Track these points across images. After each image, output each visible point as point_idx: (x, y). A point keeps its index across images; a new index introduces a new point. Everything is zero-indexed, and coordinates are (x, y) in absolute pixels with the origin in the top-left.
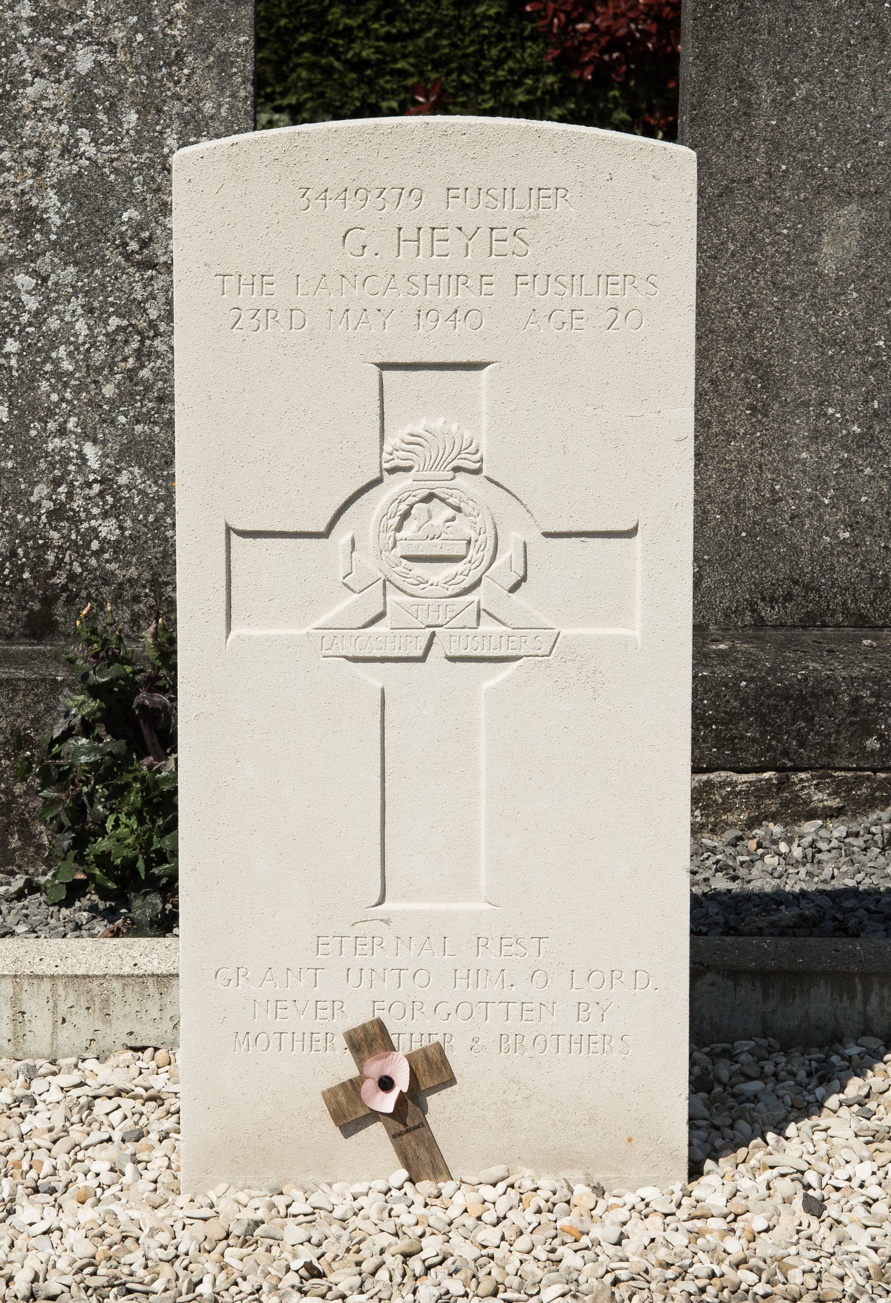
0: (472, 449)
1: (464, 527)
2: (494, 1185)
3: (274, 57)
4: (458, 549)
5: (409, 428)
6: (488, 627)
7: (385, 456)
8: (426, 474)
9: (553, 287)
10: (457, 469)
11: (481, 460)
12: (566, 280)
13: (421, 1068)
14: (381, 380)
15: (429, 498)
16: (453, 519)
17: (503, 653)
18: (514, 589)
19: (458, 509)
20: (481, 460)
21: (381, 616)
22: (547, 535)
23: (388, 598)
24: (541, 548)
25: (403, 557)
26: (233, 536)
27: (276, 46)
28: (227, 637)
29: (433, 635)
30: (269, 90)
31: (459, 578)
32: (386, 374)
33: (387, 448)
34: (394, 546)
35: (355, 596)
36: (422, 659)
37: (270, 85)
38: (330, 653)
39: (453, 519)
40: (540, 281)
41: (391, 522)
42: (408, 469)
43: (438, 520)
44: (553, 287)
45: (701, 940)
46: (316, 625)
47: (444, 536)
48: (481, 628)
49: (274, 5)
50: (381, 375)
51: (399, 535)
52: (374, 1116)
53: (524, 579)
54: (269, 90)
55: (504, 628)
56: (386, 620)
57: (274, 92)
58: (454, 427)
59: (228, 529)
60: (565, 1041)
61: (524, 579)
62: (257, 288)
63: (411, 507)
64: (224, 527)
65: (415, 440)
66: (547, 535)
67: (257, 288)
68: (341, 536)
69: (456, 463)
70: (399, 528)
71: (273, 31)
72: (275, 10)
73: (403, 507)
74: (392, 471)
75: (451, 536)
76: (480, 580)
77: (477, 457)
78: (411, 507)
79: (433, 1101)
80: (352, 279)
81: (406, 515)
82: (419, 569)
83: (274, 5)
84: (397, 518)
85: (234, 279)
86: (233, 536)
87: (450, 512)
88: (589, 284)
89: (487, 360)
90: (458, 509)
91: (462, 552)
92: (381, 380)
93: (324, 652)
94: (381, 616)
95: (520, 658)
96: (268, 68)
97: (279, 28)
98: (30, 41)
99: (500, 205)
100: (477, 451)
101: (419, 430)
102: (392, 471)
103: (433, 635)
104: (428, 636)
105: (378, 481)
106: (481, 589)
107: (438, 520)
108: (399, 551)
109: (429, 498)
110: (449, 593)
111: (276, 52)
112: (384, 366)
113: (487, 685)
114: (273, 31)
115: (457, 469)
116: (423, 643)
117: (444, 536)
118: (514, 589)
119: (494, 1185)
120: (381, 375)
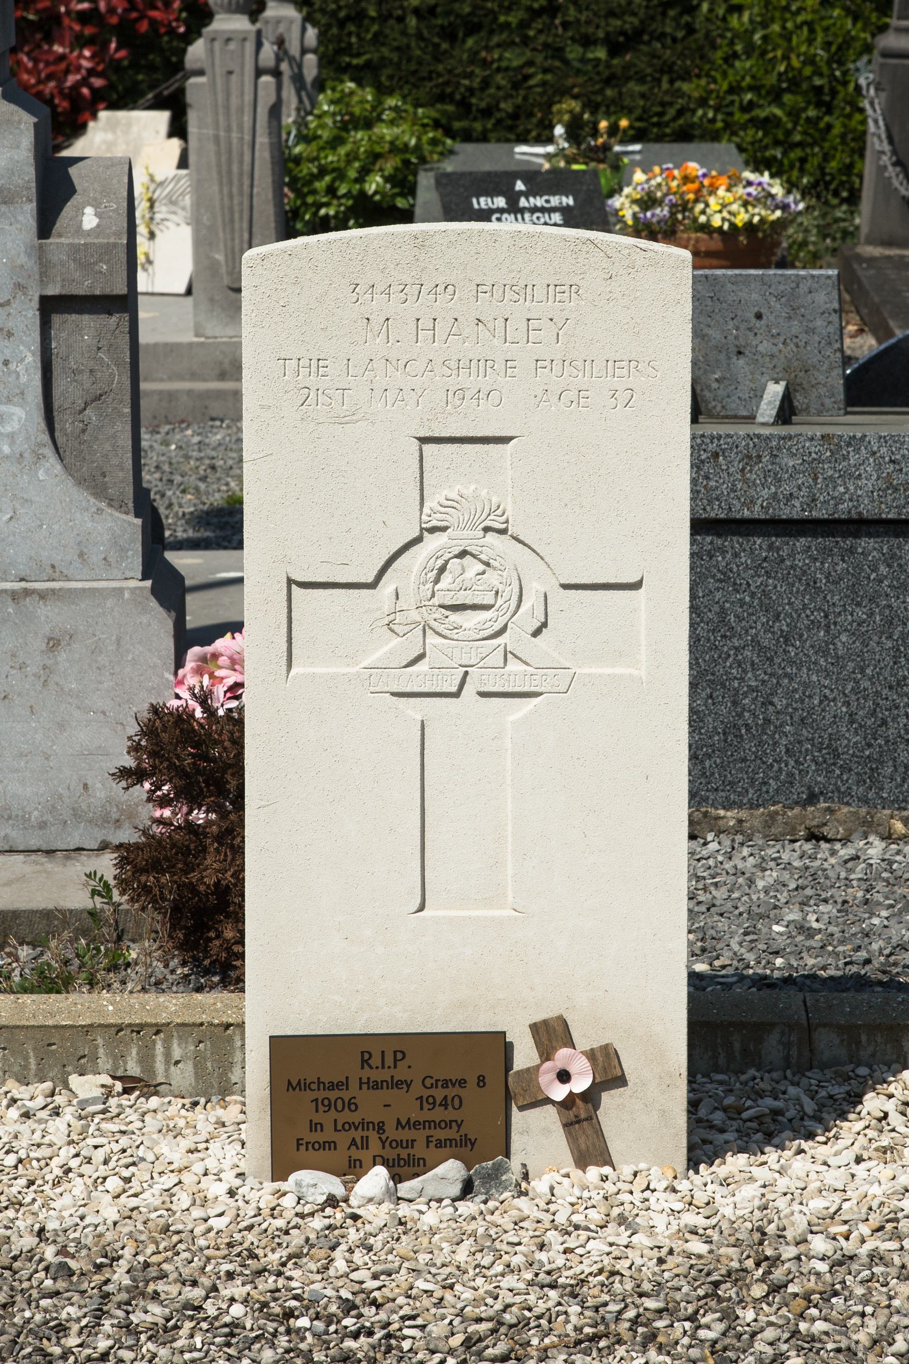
0: (499, 512)
1: (492, 578)
4: (488, 599)
5: (445, 492)
6: (514, 666)
7: (424, 518)
8: (458, 533)
9: (509, 294)
10: (487, 529)
11: (507, 522)
12: (580, 364)
15: (463, 554)
16: (483, 573)
17: (526, 689)
18: (536, 633)
19: (488, 564)
20: (507, 522)
21: (421, 657)
22: (566, 587)
23: (427, 641)
24: (560, 598)
25: (441, 606)
26: (294, 587)
29: (466, 673)
31: (489, 624)
32: (426, 447)
33: (426, 510)
34: (433, 596)
35: (399, 639)
36: (457, 695)
38: (377, 689)
39: (483, 573)
40: (557, 367)
41: (430, 575)
42: (444, 529)
43: (470, 573)
44: (509, 294)
46: (362, 665)
47: (475, 587)
48: (507, 668)
50: (421, 450)
51: (437, 587)
52: (548, 1101)
53: (545, 625)
55: (525, 667)
56: (426, 660)
58: (484, 493)
59: (290, 582)
61: (545, 625)
62: (314, 369)
63: (447, 562)
64: (285, 580)
65: (450, 504)
66: (566, 587)
67: (314, 369)
68: (387, 587)
69: (488, 523)
70: (437, 581)
73: (440, 562)
74: (433, 530)
75: (481, 588)
76: (506, 626)
77: (505, 517)
78: (447, 562)
79: (606, 1097)
80: (394, 362)
81: (442, 570)
82: (455, 618)
84: (435, 572)
85: (294, 362)
86: (294, 587)
87: (481, 567)
88: (540, 293)
89: (509, 434)
90: (488, 564)
91: (492, 602)
93: (372, 689)
94: (421, 657)
95: (540, 694)
99: (581, 374)
100: (503, 514)
101: (454, 495)
102: (433, 530)
103: (466, 673)
104: (461, 675)
105: (418, 540)
106: (506, 635)
107: (470, 573)
108: (436, 601)
109: (463, 554)
110: (479, 637)
112: (424, 440)
113: (512, 718)
115: (487, 529)
116: (457, 682)
117: (475, 587)
118: (536, 633)
120: (421, 450)
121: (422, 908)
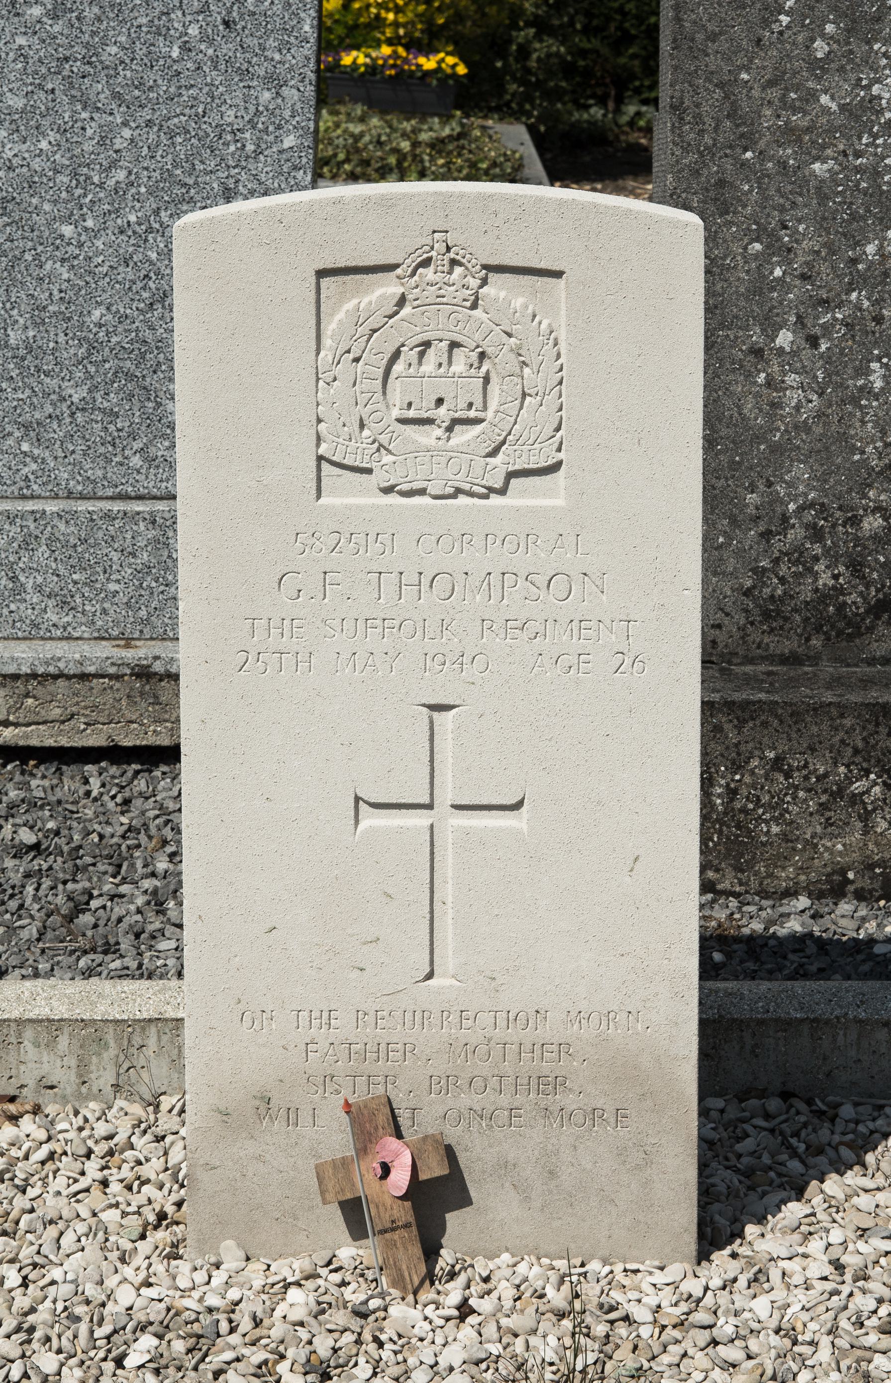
2: (477, 1364)
3: (643, 53)
13: (416, 1152)
14: (431, 723)
27: (645, 42)
28: (356, 828)
30: (637, 83)
37: (636, 78)
45: (709, 984)
49: (646, 4)
54: (637, 83)
57: (642, 86)
59: (357, 799)
60: (260, 624)
71: (643, 28)
72: (646, 8)
83: (646, 4)
92: (431, 723)
96: (636, 63)
97: (649, 25)
98: (277, 57)
111: (645, 48)
114: (643, 28)
119: (477, 1364)
121: (430, 976)
